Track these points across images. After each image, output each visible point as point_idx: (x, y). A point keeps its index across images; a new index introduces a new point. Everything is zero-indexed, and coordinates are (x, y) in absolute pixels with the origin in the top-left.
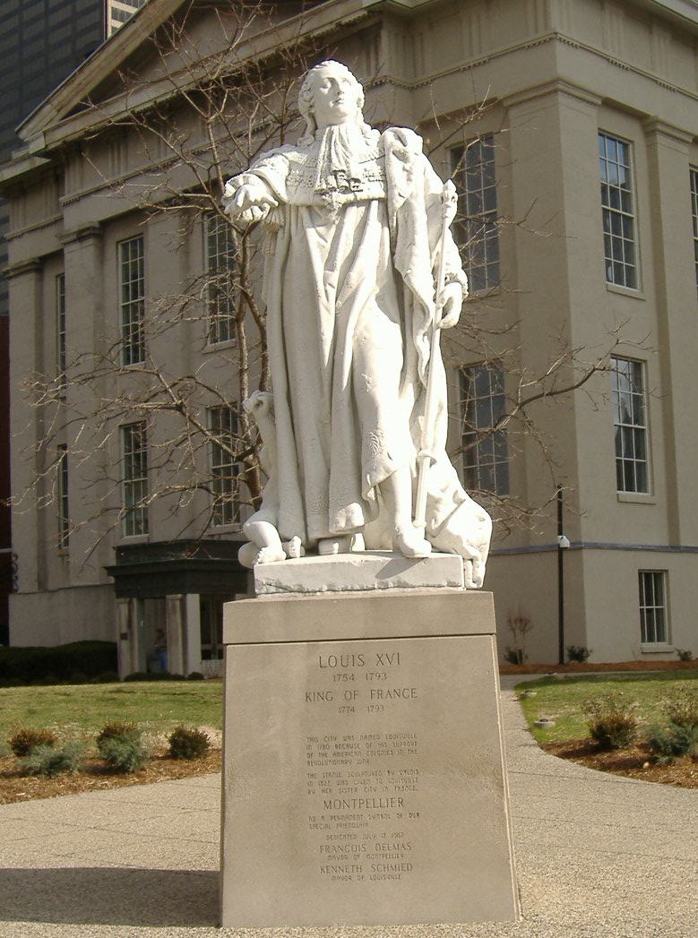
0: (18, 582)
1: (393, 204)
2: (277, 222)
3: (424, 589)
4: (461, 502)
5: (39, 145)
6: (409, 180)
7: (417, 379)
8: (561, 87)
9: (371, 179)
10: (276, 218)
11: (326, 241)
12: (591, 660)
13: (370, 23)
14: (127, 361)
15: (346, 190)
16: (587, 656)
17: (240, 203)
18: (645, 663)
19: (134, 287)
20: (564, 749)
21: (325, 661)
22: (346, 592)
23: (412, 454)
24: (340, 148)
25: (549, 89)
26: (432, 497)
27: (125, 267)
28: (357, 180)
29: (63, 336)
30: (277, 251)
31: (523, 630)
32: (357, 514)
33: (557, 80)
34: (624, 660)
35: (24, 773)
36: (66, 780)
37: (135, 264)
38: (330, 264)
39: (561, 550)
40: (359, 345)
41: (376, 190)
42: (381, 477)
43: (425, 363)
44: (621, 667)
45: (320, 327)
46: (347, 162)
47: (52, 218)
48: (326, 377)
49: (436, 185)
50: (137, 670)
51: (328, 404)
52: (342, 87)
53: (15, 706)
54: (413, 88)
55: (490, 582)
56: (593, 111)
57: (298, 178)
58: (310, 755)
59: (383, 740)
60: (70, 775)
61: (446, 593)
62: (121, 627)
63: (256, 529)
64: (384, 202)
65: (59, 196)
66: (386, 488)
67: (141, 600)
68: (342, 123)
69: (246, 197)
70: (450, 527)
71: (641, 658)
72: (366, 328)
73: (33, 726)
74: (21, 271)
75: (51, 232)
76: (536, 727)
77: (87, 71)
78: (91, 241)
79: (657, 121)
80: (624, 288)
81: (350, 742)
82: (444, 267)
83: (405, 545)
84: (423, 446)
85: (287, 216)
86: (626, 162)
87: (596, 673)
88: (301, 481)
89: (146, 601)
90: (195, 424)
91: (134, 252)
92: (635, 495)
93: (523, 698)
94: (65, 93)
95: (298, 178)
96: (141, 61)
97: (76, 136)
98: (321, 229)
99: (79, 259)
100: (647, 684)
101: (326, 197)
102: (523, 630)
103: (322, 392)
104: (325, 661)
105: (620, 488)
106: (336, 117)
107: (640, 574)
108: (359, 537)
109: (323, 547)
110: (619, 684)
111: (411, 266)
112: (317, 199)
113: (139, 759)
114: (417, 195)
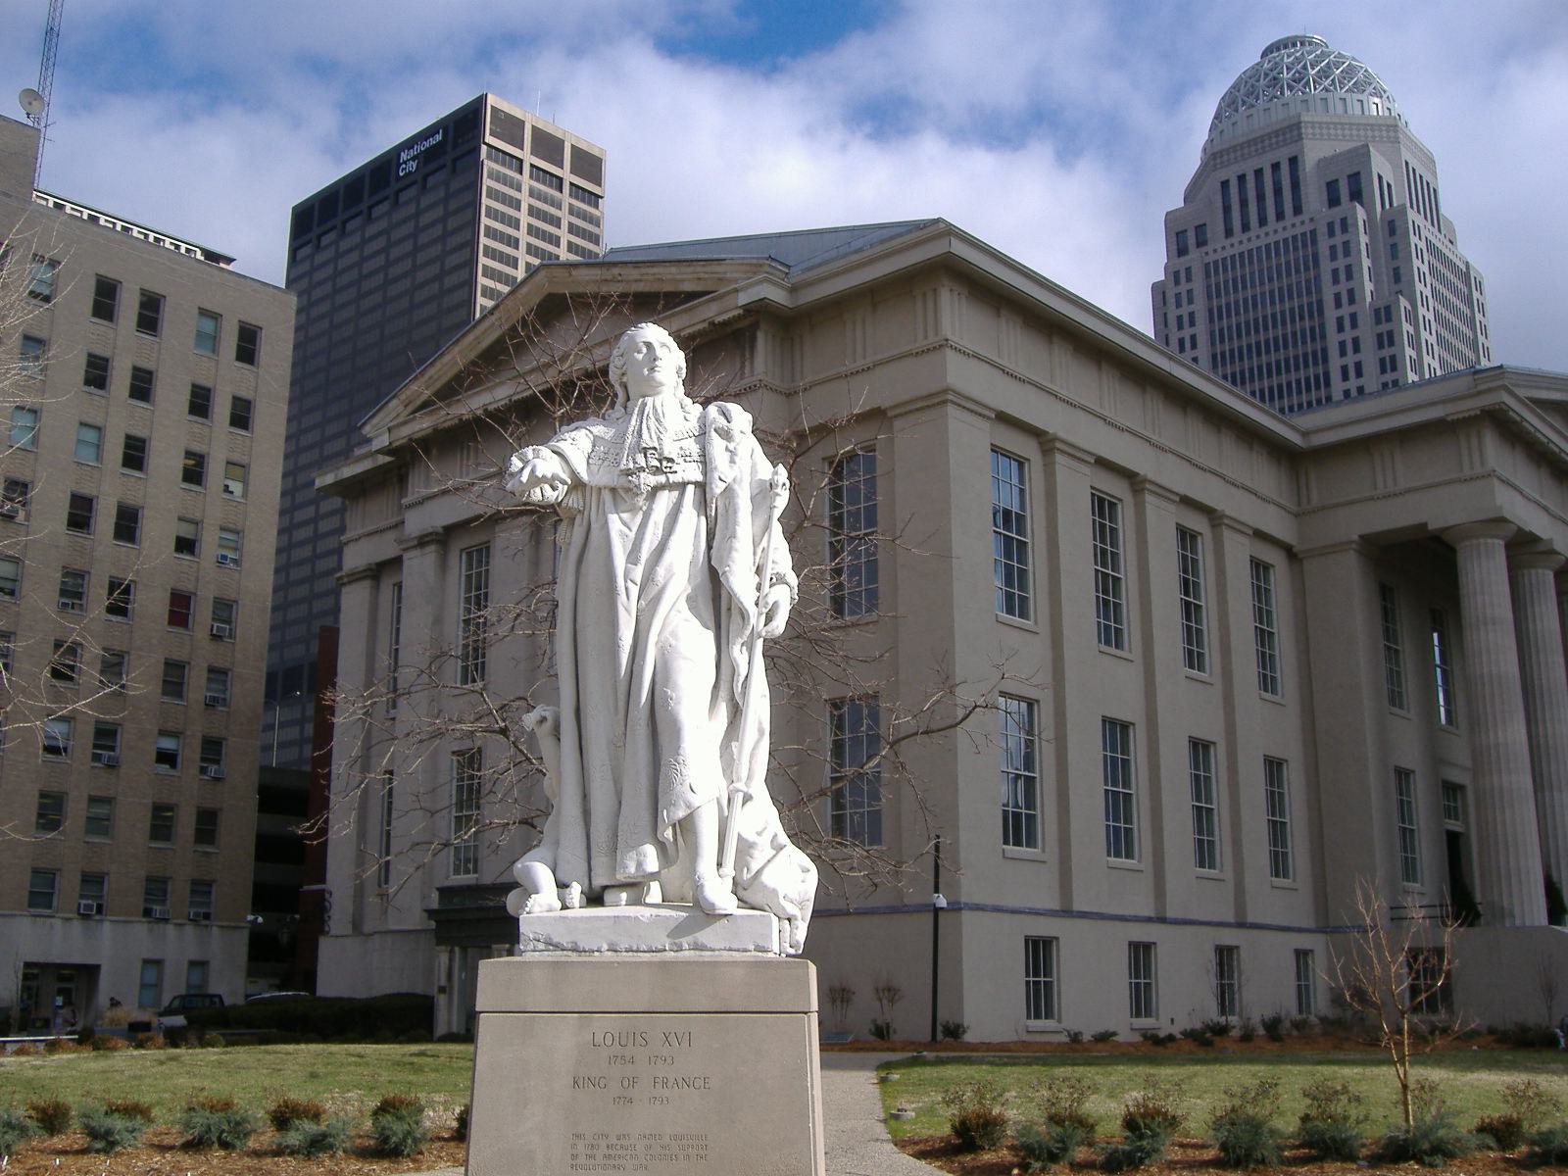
0: (331, 923)
1: (712, 489)
2: (575, 505)
3: (725, 953)
4: (779, 848)
5: (383, 441)
6: (732, 461)
7: (732, 698)
8: (950, 397)
9: (688, 459)
10: (574, 502)
11: (630, 530)
12: (968, 1037)
13: (747, 322)
14: (465, 681)
15: (658, 471)
16: (964, 1032)
17: (525, 478)
18: (1030, 1043)
19: (478, 593)
20: (922, 1147)
21: (599, 1039)
22: (631, 954)
23: (721, 788)
24: (653, 423)
25: (937, 400)
26: (746, 841)
27: (469, 578)
28: (670, 460)
29: (397, 650)
30: (574, 539)
31: (892, 1001)
32: (651, 859)
33: (946, 391)
34: (1006, 1039)
35: (279, 1152)
36: (327, 1163)
37: (479, 574)
38: (633, 557)
39: (937, 911)
40: (664, 654)
41: (694, 473)
42: (681, 814)
43: (742, 679)
44: (1003, 1047)
45: (618, 631)
46: (659, 439)
47: (396, 519)
48: (622, 689)
49: (765, 469)
50: (455, 1030)
51: (622, 723)
52: (659, 352)
53: (296, 1067)
54: (790, 394)
55: (812, 949)
56: (986, 425)
57: (602, 455)
58: (574, 1157)
59: (666, 1140)
60: (332, 1157)
61: (752, 959)
62: (439, 980)
63: (528, 871)
64: (702, 487)
65: (401, 497)
66: (687, 827)
67: (464, 949)
68: (658, 393)
69: (533, 471)
70: (765, 878)
71: (1026, 1037)
72: (674, 634)
73: (297, 1096)
74: (356, 577)
75: (391, 536)
76: (893, 1118)
77: (438, 365)
78: (433, 548)
79: (1055, 439)
80: (1016, 620)
81: (624, 1142)
82: (770, 565)
83: (704, 897)
84: (735, 779)
85: (588, 499)
86: (1021, 481)
87: (970, 1054)
88: (586, 814)
89: (469, 950)
90: (521, 751)
91: (480, 562)
92: (1023, 851)
93: (883, 1081)
94: (414, 387)
95: (602, 455)
96: (494, 359)
97: (423, 433)
98: (625, 516)
99: (419, 567)
100: (1029, 1069)
101: (633, 479)
102: (892, 1001)
103: (616, 708)
104: (599, 1039)
105: (1006, 842)
106: (652, 387)
107: (1027, 941)
108: (655, 886)
109: (608, 897)
110: (996, 1069)
111: (731, 563)
112: (623, 481)
113: (416, 1141)
114: (741, 480)
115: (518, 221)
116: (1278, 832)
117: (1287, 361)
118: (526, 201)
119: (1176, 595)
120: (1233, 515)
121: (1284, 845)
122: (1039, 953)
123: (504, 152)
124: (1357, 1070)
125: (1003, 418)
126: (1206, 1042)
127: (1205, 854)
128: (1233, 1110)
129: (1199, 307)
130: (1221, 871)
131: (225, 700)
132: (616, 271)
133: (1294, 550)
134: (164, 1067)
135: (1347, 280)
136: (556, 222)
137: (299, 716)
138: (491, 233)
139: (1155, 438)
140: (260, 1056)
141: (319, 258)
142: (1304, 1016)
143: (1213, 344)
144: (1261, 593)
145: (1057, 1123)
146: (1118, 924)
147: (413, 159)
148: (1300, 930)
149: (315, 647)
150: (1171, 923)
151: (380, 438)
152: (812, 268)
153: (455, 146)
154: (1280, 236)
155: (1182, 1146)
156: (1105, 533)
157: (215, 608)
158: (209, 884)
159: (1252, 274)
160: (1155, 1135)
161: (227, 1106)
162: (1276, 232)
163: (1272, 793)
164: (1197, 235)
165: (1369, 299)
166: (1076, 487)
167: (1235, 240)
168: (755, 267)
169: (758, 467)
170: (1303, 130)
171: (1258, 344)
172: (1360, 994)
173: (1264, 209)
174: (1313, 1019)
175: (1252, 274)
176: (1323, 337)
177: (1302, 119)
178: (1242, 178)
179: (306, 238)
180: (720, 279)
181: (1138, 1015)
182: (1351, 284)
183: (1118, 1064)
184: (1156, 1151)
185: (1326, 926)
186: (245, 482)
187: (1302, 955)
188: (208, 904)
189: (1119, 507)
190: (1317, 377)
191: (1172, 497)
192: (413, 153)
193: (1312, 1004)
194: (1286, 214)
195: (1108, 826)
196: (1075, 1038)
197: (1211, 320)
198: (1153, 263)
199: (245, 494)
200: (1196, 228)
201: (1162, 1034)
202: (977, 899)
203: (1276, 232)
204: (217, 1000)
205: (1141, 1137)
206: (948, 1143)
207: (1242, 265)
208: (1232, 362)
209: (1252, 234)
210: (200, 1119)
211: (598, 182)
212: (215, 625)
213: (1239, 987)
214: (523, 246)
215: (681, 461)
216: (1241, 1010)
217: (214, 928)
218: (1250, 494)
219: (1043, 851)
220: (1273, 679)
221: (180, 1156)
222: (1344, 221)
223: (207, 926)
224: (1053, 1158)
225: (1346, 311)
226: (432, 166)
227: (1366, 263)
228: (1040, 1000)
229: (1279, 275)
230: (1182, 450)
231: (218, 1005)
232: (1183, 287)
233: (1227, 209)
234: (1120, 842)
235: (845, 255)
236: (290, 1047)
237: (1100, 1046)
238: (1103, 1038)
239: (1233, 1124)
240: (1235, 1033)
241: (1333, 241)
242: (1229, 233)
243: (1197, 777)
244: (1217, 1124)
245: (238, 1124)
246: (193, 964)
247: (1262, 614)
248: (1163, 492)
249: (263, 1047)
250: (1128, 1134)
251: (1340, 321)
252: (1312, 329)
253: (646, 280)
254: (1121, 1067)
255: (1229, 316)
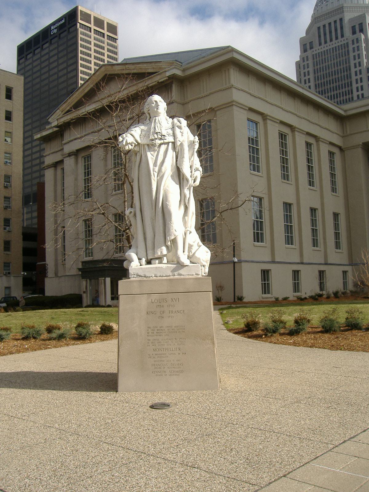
0: (48, 274)
3: (187, 276)
4: (200, 246)
5: (55, 123)
6: (182, 135)
7: (185, 204)
8: (234, 104)
9: (169, 135)
10: (137, 149)
12: (245, 300)
14: (85, 198)
15: (161, 139)
16: (243, 299)
17: (124, 144)
18: (263, 301)
19: (88, 172)
20: (235, 331)
21: (153, 301)
23: (183, 230)
24: (158, 125)
25: (230, 104)
26: (190, 244)
27: (85, 166)
28: (164, 136)
29: (63, 189)
30: (137, 160)
31: (221, 290)
32: (164, 250)
35: (50, 339)
36: (64, 342)
37: (88, 164)
38: (155, 164)
39: (234, 263)
41: (171, 139)
42: (173, 238)
43: (188, 198)
44: (255, 303)
45: (152, 186)
46: (161, 130)
47: (60, 149)
49: (191, 137)
50: (89, 304)
51: (154, 212)
52: (159, 104)
53: (47, 316)
55: (210, 273)
56: (245, 112)
57: (144, 135)
58: (148, 333)
59: (173, 328)
60: (66, 340)
62: (83, 289)
63: (130, 256)
64: (174, 143)
66: (174, 241)
67: (90, 280)
69: (126, 141)
70: (196, 255)
71: (262, 300)
73: (53, 323)
74: (49, 167)
76: (226, 323)
77: (72, 98)
78: (73, 157)
79: (267, 115)
80: (256, 173)
81: (162, 329)
82: (194, 165)
84: (187, 227)
85: (140, 148)
86: (257, 129)
88: (145, 239)
91: (88, 160)
92: (260, 244)
93: (221, 313)
94: (64, 106)
95: (144, 135)
96: (90, 95)
97: (68, 120)
98: (152, 152)
99: (69, 163)
100: (264, 308)
101: (154, 142)
102: (221, 290)
103: (152, 208)
104: (153, 301)
105: (255, 241)
106: (157, 114)
107: (261, 271)
108: (165, 258)
109: (153, 262)
110: (254, 309)
111: (183, 165)
112: (151, 142)
113: (90, 334)
115: (91, 48)
116: (337, 235)
117: (339, 86)
118: (93, 42)
119: (305, 163)
120: (322, 137)
121: (339, 239)
122: (265, 274)
123: (85, 26)
124: (362, 305)
125: (251, 110)
126: (316, 299)
127: (315, 243)
128: (326, 317)
129: (311, 69)
130: (320, 248)
131: (10, 207)
132: (127, 66)
133: (342, 148)
134: (7, 318)
135: (358, 59)
136: (103, 48)
137: (30, 210)
138: (82, 53)
139: (298, 114)
140: (35, 313)
141: (27, 63)
142: (345, 291)
143: (315, 81)
144: (332, 162)
145: (275, 323)
146: (289, 265)
147: (55, 28)
148: (344, 265)
149: (35, 188)
150: (305, 264)
151: (54, 123)
152: (188, 63)
153: (69, 24)
154: (337, 45)
155: (312, 328)
156: (283, 145)
157: (5, 178)
158: (9, 263)
159: (328, 57)
160: (303, 324)
161: (33, 327)
162: (335, 44)
163: (335, 223)
164: (310, 45)
165: (365, 65)
166: (274, 131)
167: (322, 46)
168: (171, 64)
169: (189, 137)
170: (344, 9)
171: (330, 80)
172: (362, 283)
173: (332, 35)
174: (348, 292)
175: (328, 57)
176: (351, 78)
177: (344, 6)
178: (324, 26)
179: (22, 56)
180: (160, 68)
181: (295, 292)
182: (359, 60)
183: (291, 306)
184: (304, 329)
185: (352, 263)
186: (11, 138)
187: (345, 273)
188: (9, 270)
189: (287, 136)
190: (349, 91)
191: (304, 132)
192: (55, 26)
193: (348, 287)
194: (339, 38)
195: (285, 235)
196: (277, 299)
197: (315, 73)
198: (296, 55)
199: (12, 142)
200: (310, 43)
201: (303, 297)
202: (247, 259)
203: (335, 44)
204: (15, 298)
205: (300, 325)
206: (243, 329)
207: (325, 55)
208: (322, 87)
209: (328, 44)
210: (26, 331)
211: (116, 34)
212: (5, 183)
213: (326, 283)
214: (93, 56)
215: (167, 136)
216: (326, 289)
217: (12, 277)
218: (328, 131)
219: (266, 243)
220: (336, 188)
221: (22, 342)
222: (357, 39)
223: (9, 276)
224: (274, 332)
225: (358, 69)
226: (61, 31)
227: (364, 53)
228: (266, 288)
229: (337, 58)
230: (306, 117)
231: (15, 299)
232: (306, 63)
233: (320, 36)
234: (289, 240)
235: (200, 59)
236: (43, 311)
237: (284, 301)
238: (285, 299)
239: (326, 321)
240: (325, 296)
241: (356, 69)
242: (320, 44)
243: (312, 219)
244: (321, 322)
245: (38, 331)
246: (6, 288)
247: (332, 168)
248: (301, 131)
249: (35, 311)
250: (296, 324)
251: (356, 72)
252: (347, 75)
253: (136, 69)
254: (292, 307)
255: (320, 72)
